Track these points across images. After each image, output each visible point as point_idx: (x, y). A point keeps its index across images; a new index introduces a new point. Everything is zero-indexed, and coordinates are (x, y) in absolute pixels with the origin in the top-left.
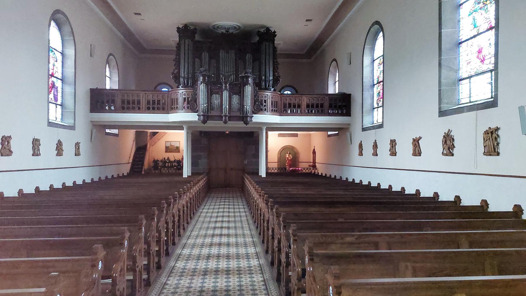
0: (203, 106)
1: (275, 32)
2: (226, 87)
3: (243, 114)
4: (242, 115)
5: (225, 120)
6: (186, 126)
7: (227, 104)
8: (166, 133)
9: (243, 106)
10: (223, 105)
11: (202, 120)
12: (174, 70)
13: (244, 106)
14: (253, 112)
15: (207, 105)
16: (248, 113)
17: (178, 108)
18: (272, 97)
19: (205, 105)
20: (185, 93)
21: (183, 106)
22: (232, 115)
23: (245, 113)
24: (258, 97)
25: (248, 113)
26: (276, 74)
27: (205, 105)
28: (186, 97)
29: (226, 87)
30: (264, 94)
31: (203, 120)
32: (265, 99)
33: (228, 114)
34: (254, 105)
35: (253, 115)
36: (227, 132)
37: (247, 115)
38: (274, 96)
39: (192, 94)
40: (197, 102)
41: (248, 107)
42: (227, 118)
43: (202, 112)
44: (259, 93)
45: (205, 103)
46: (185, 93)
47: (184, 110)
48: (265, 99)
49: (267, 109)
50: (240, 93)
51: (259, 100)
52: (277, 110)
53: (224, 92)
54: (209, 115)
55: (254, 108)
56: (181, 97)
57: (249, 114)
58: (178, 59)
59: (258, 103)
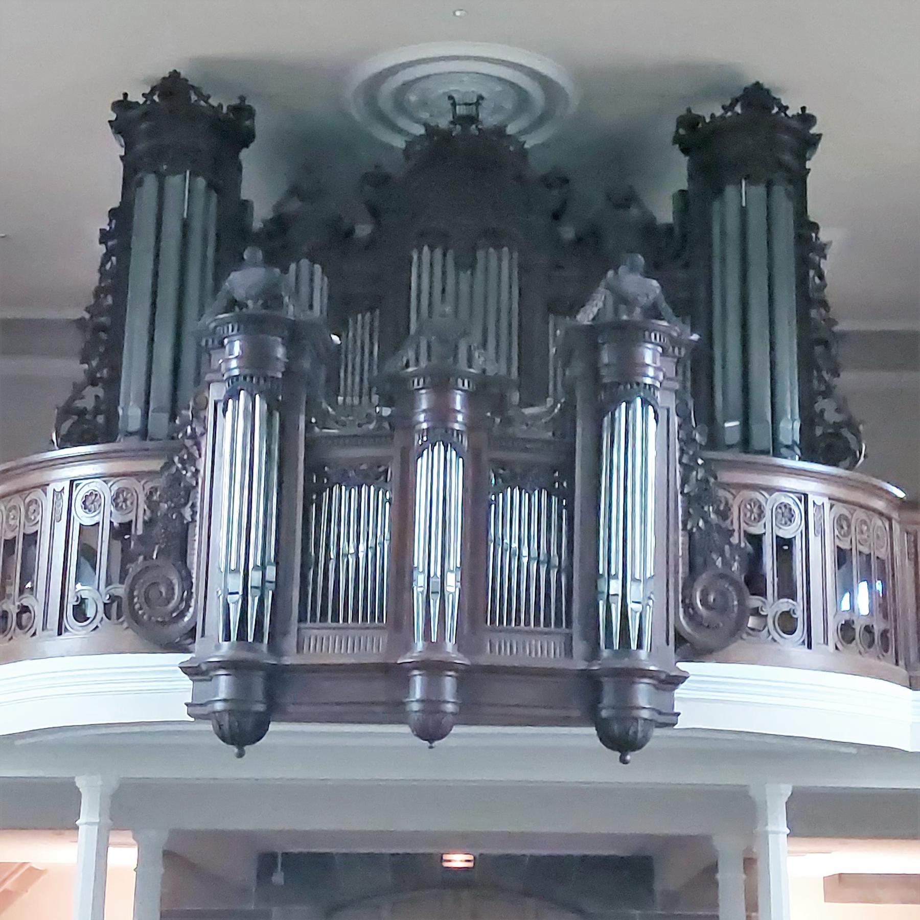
0: (236, 583)
1: (807, 119)
2: (441, 414)
3: (594, 653)
4: (582, 665)
5: (432, 703)
6: (98, 781)
7: (454, 560)
8: (32, 874)
9: (593, 578)
10: (412, 569)
11: (219, 706)
12: (78, 391)
13: (602, 586)
14: (680, 639)
15: (271, 573)
16: (640, 646)
17: (32, 619)
18: (841, 522)
19: (255, 578)
20: (97, 485)
21: (71, 601)
22: (486, 659)
23: (609, 645)
24: (724, 515)
25: (640, 646)
26: (822, 404)
27: (255, 578)
28: (98, 519)
29: (441, 414)
30: (771, 490)
31: (230, 712)
32: (781, 534)
33: (460, 646)
34: (688, 585)
35: (683, 666)
36: (458, 860)
37: (625, 663)
38: (860, 514)
39: (149, 497)
40: (194, 560)
41: (635, 592)
42: (449, 684)
43: (227, 638)
44: (727, 476)
45: (255, 558)
46: (97, 485)
47: (77, 633)
48: (785, 533)
49: (799, 615)
50: (568, 471)
51: (735, 540)
52: (884, 634)
53: (422, 463)
54: (288, 660)
55: (688, 606)
56: (61, 527)
57: (643, 654)
58: (110, 310)
59: (727, 564)
